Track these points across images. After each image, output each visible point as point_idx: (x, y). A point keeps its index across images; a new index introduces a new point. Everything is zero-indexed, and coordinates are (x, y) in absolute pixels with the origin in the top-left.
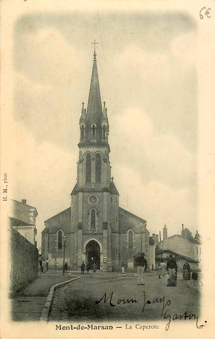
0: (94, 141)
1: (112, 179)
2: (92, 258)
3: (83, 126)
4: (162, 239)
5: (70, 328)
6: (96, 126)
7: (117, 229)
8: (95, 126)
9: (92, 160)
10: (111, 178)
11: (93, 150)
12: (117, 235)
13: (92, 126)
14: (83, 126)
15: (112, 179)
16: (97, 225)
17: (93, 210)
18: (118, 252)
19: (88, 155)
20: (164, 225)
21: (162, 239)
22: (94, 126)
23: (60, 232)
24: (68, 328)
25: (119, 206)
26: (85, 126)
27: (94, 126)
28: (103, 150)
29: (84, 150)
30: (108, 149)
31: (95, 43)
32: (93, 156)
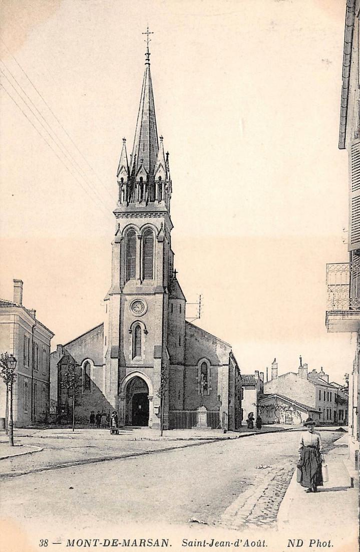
0: (141, 206)
1: (175, 272)
2: (140, 407)
3: (122, 179)
4: (269, 379)
5: (202, 544)
6: (145, 179)
7: (180, 358)
8: (143, 179)
9: (138, 238)
10: (174, 271)
11: (139, 222)
12: (181, 368)
13: (138, 179)
14: (122, 179)
15: (175, 272)
16: (144, 351)
17: (139, 326)
18: (182, 396)
19: (130, 232)
20: (350, 480)
21: (269, 379)
22: (141, 178)
23: (87, 362)
24: (197, 544)
25: (186, 319)
26: (125, 180)
27: (141, 178)
28: (157, 222)
29: (124, 222)
30: (166, 218)
31: (148, 33)
32: (138, 233)
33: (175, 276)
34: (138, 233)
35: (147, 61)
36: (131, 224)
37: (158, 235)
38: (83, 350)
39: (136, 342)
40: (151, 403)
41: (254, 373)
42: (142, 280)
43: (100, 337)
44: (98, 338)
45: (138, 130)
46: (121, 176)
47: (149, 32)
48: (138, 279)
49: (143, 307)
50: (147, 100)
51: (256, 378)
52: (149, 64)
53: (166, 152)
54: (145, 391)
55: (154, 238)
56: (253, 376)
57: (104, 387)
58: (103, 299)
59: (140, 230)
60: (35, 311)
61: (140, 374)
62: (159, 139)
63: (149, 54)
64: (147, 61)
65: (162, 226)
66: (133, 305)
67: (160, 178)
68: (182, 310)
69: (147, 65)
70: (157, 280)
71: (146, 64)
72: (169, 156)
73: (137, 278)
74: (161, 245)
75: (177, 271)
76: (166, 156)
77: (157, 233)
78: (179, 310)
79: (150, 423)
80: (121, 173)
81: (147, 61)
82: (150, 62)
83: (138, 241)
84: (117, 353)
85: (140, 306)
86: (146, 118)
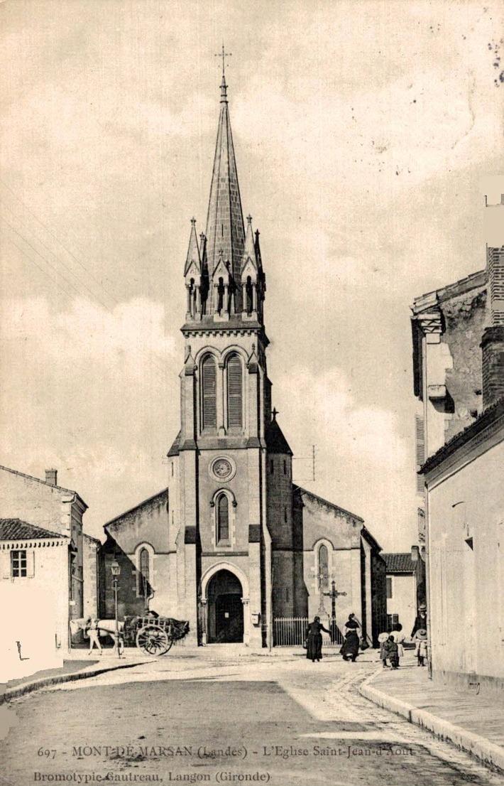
1: (275, 413)
3: (192, 281)
6: (226, 281)
9: (220, 367)
10: (272, 410)
11: (220, 343)
14: (192, 281)
15: (275, 413)
22: (221, 280)
31: (223, 55)
32: (218, 359)
33: (274, 418)
34: (218, 359)
35: (223, 99)
36: (208, 346)
37: (249, 361)
38: (137, 530)
39: (222, 522)
40: (245, 607)
41: (409, 551)
42: (226, 429)
43: (163, 510)
44: (159, 511)
45: (213, 203)
46: (190, 276)
47: (221, 53)
48: (221, 428)
49: (229, 469)
50: (224, 158)
51: (414, 558)
52: (227, 102)
53: (254, 231)
54: (236, 592)
55: (243, 368)
56: (409, 555)
57: (469, 295)
58: (166, 454)
59: (221, 353)
60: (56, 472)
61: (214, 568)
62: (245, 220)
63: (225, 87)
64: (223, 99)
65: (254, 349)
66: (216, 462)
67: (249, 278)
68: (287, 470)
69: (224, 104)
70: (250, 426)
71: (221, 102)
72: (259, 236)
73: (218, 427)
74: (254, 376)
75: (277, 411)
76: (255, 236)
77: (247, 359)
78: (282, 468)
79: (246, 638)
80: (189, 271)
81: (224, 97)
82: (227, 100)
83: (219, 371)
84: (192, 536)
85: (223, 466)
86: (224, 186)
